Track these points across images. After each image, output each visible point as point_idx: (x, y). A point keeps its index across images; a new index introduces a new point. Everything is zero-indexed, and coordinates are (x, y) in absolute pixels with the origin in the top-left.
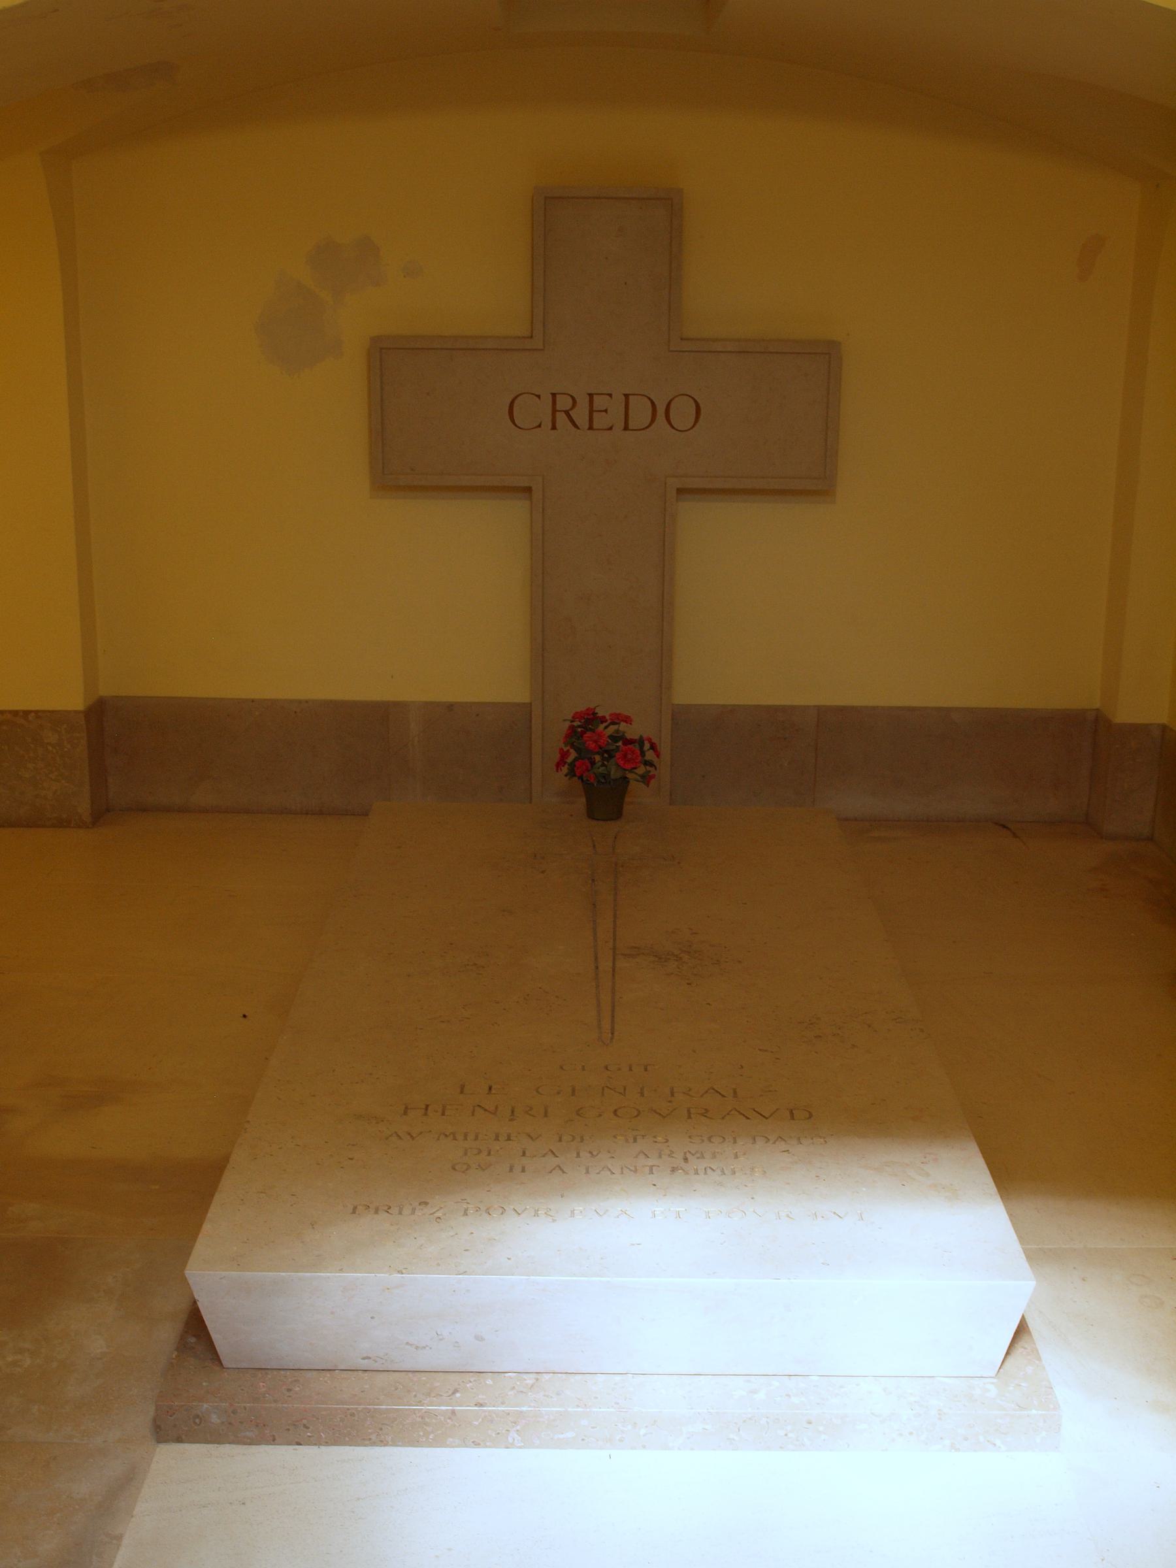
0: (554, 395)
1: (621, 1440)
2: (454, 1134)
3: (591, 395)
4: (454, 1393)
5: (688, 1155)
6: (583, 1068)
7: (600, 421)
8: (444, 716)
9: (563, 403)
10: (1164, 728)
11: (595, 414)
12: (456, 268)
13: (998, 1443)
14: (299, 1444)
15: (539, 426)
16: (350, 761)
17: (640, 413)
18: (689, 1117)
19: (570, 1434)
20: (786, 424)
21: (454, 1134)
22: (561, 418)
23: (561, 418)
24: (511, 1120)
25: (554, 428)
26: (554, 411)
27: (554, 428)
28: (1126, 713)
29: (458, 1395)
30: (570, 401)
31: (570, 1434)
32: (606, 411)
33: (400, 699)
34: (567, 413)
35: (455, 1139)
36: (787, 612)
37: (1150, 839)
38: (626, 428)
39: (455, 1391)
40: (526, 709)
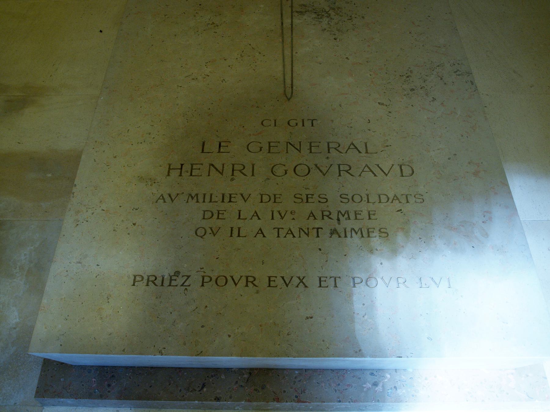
4: (203, 388)
5: (340, 216)
24: (232, 180)
29: (205, 389)
39: (204, 386)
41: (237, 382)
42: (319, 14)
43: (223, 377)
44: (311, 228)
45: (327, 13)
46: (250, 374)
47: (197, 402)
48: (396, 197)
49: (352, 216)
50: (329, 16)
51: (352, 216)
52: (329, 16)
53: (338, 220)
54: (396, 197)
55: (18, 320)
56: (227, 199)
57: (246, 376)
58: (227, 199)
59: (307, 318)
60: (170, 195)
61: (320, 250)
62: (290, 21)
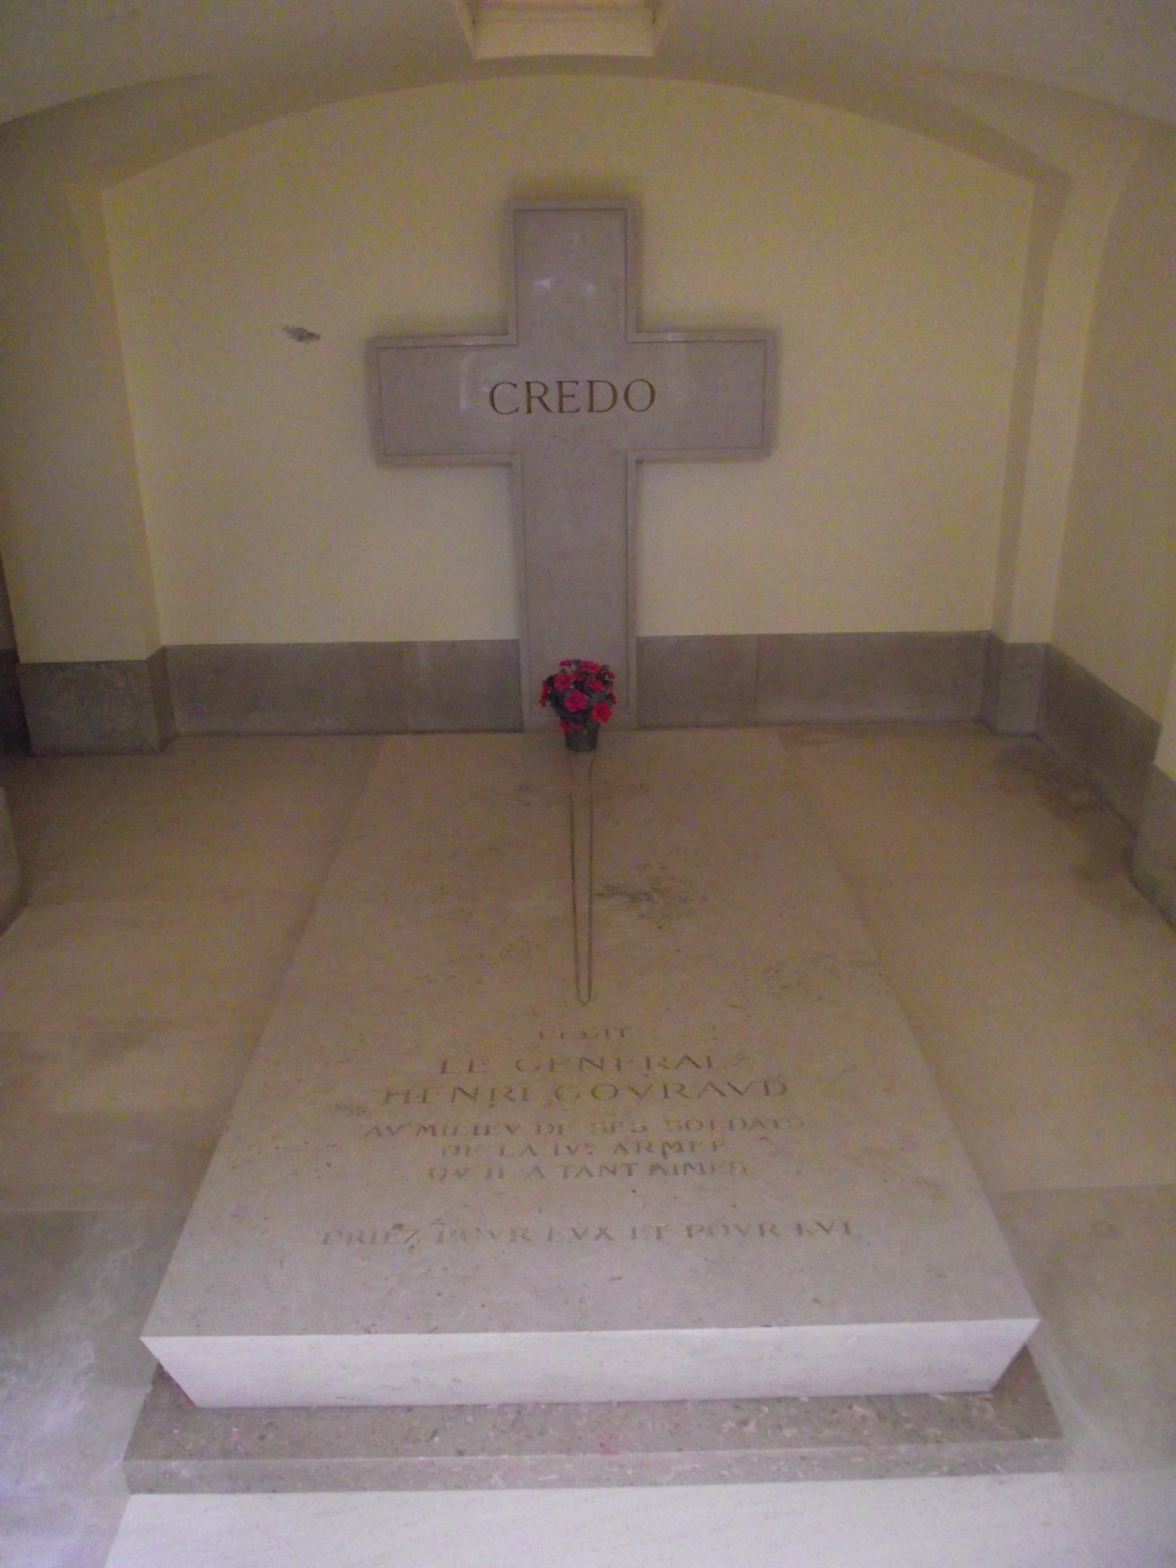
0: (528, 383)
1: (608, 1480)
2: (433, 1127)
3: (560, 383)
4: (432, 1437)
5: (667, 1149)
6: (562, 1036)
7: (569, 404)
8: (451, 655)
9: (537, 390)
10: (1048, 647)
11: (564, 399)
12: (441, 279)
13: (998, 1467)
14: (274, 1491)
15: (517, 410)
16: (375, 698)
17: (603, 396)
18: (666, 1096)
19: (553, 1477)
20: (735, 394)
21: (433, 1127)
22: (535, 403)
23: (535, 403)
24: (492, 1106)
25: (529, 411)
26: (529, 398)
27: (529, 411)
28: (1017, 633)
29: (437, 1439)
30: (542, 389)
31: (553, 1477)
32: (573, 396)
33: (409, 639)
34: (540, 398)
35: (434, 1134)
36: (722, 559)
37: (1034, 735)
38: (591, 410)
39: (435, 1433)
40: (515, 642)
41: (494, 1427)
42: (634, 898)
43: (470, 1419)
44: (584, 413)
45: (646, 894)
46: (519, 1412)
47: (421, 1458)
48: (757, 1122)
49: (686, 1147)
50: (650, 899)
51: (686, 1147)
52: (650, 899)
53: (664, 1153)
54: (757, 1122)
55: (92, 1361)
56: (482, 1131)
57: (511, 1417)
58: (482, 1131)
59: (613, 1279)
60: (389, 1128)
61: (634, 1191)
62: (586, 906)
